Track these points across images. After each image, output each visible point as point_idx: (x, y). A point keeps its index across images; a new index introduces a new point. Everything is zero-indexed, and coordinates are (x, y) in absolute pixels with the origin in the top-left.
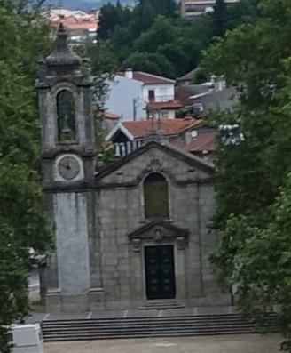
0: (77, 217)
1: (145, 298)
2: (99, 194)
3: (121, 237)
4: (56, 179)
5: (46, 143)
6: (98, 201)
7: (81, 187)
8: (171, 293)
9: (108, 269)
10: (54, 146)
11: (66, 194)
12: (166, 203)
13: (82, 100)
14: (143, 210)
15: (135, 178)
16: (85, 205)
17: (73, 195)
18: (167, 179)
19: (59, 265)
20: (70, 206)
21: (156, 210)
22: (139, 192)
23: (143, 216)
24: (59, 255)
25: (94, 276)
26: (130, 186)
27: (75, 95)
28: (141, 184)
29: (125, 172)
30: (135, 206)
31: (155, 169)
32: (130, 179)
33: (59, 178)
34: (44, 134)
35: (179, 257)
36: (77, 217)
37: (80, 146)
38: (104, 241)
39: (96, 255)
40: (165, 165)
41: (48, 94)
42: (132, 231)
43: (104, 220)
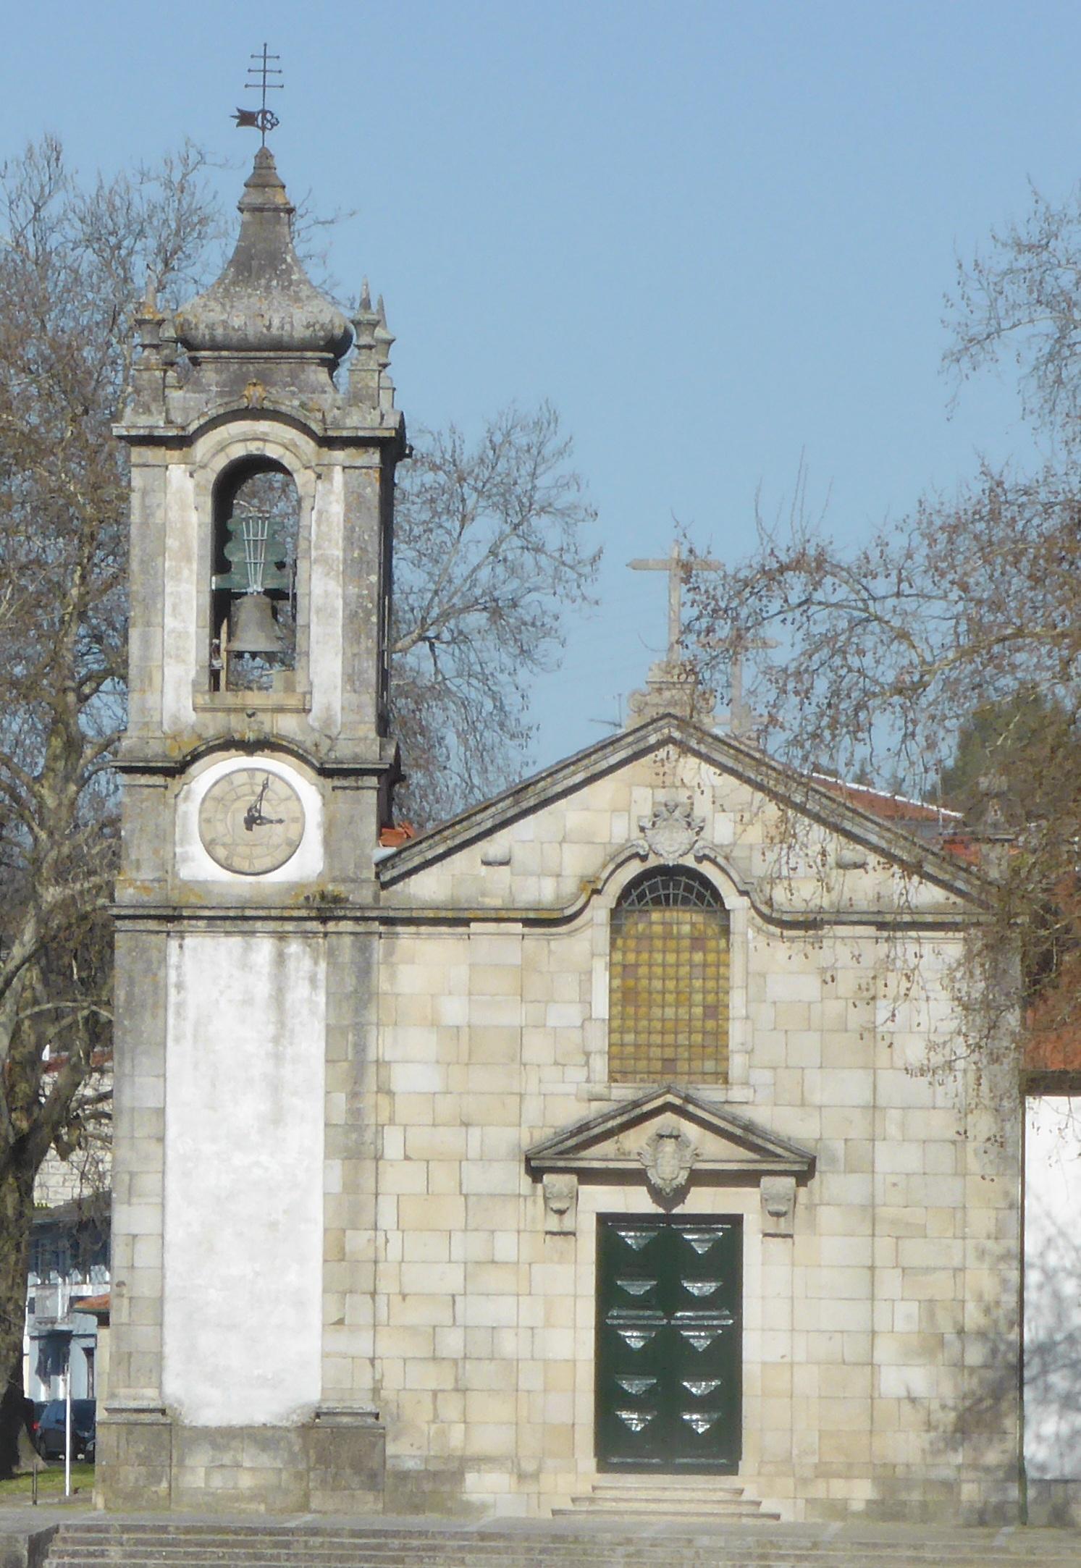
0: (278, 1058)
1: (588, 1461)
2: (390, 952)
3: (485, 1159)
4: (185, 873)
5: (152, 700)
6: (382, 980)
7: (323, 909)
8: (722, 1450)
9: (416, 1315)
10: (191, 717)
11: (236, 941)
12: (716, 1011)
13: (337, 509)
14: (599, 1040)
15: (570, 886)
16: (321, 998)
17: (264, 948)
18: (732, 900)
19: (170, 1282)
20: (248, 1001)
21: (667, 1051)
22: (592, 934)
23: (600, 1066)
24: (175, 1234)
25: (342, 1342)
26: (545, 920)
27: (303, 478)
28: (600, 910)
29: (519, 855)
30: (565, 1015)
31: (671, 847)
32: (543, 892)
33: (199, 867)
34: (145, 658)
35: (761, 1265)
36: (278, 1058)
37: (312, 719)
38: (399, 1178)
39: (358, 1241)
40: (721, 830)
41: (177, 473)
42: (543, 1135)
43: (405, 1079)
